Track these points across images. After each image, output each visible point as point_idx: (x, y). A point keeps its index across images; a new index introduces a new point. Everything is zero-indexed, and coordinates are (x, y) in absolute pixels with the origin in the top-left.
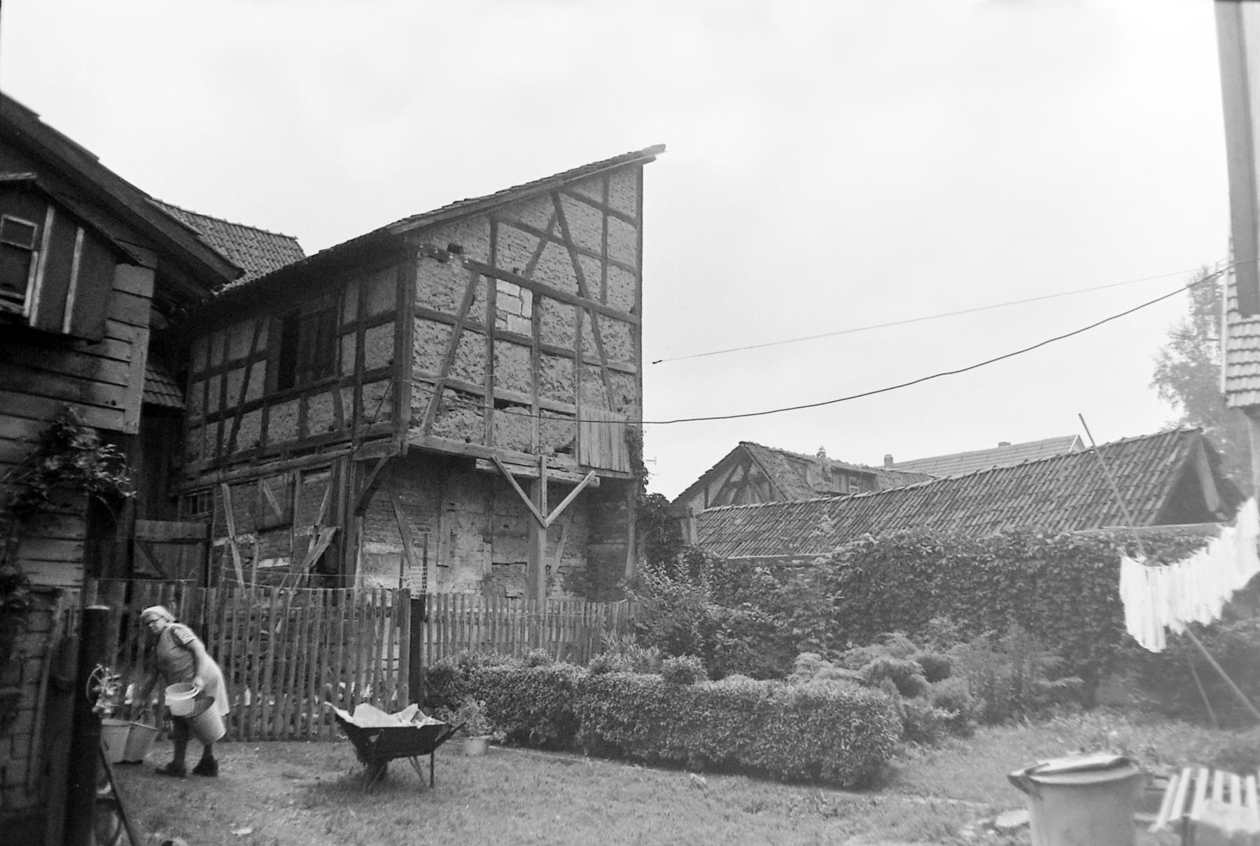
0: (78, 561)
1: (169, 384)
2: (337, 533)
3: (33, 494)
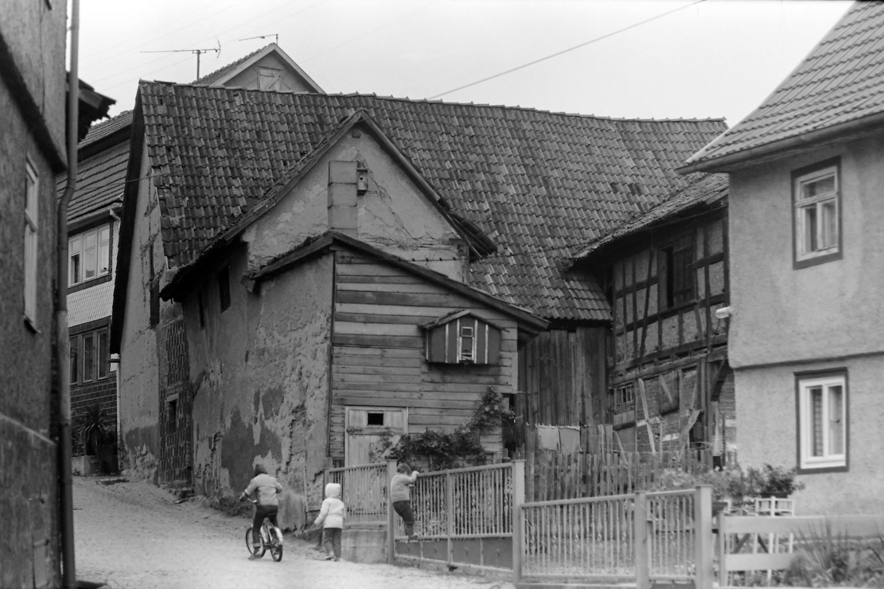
0: (500, 442)
1: (601, 300)
2: (701, 415)
3: (482, 420)
